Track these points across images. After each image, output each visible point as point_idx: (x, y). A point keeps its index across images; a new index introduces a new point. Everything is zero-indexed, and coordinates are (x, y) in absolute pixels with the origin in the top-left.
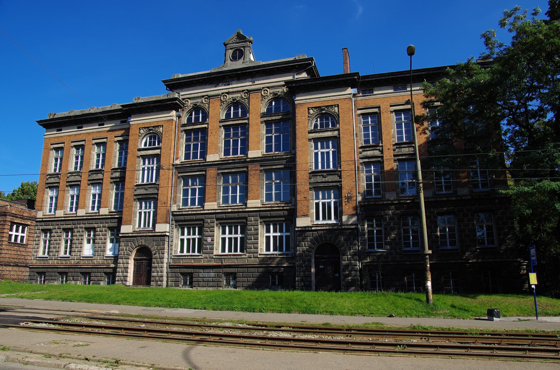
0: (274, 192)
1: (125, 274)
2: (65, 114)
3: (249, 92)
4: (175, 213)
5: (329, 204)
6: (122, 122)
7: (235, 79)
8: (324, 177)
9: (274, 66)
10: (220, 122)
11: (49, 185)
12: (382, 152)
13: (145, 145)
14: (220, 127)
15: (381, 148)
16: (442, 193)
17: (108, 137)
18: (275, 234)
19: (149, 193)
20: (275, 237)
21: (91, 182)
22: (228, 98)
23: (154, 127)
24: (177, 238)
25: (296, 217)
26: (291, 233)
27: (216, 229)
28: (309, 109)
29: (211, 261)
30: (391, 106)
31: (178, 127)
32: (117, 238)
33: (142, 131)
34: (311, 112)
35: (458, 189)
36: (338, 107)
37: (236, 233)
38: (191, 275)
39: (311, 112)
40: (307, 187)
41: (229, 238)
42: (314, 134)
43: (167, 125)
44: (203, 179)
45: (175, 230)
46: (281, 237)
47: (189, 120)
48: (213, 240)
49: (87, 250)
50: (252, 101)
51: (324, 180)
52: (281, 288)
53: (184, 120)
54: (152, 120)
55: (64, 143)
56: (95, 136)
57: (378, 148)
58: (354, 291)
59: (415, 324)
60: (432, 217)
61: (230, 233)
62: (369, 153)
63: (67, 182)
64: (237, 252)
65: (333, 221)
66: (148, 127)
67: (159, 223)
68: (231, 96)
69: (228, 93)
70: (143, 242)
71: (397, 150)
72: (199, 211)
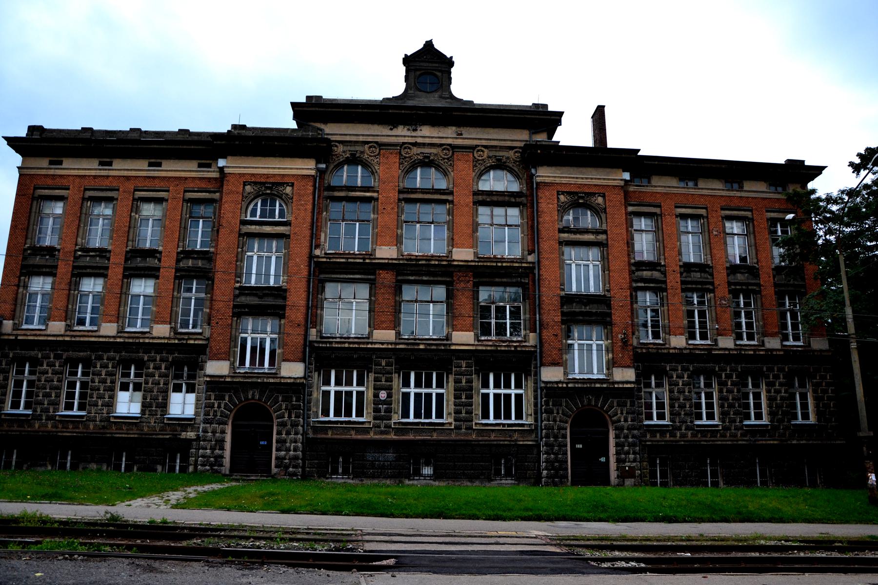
0: (493, 321)
1: (217, 452)
3: (453, 147)
4: (316, 345)
5: (263, 341)
6: (51, 163)
8: (260, 297)
12: (664, 274)
18: (418, 390)
23: (273, 184)
24: (318, 388)
26: (367, 388)
28: (558, 194)
30: (722, 209)
31: (319, 191)
35: (766, 339)
43: (303, 183)
48: (390, 396)
49: (127, 404)
54: (271, 171)
56: (92, 184)
57: (659, 268)
58: (27, 469)
59: (169, 519)
60: (109, 381)
66: (261, 183)
68: (419, 150)
71: (684, 275)
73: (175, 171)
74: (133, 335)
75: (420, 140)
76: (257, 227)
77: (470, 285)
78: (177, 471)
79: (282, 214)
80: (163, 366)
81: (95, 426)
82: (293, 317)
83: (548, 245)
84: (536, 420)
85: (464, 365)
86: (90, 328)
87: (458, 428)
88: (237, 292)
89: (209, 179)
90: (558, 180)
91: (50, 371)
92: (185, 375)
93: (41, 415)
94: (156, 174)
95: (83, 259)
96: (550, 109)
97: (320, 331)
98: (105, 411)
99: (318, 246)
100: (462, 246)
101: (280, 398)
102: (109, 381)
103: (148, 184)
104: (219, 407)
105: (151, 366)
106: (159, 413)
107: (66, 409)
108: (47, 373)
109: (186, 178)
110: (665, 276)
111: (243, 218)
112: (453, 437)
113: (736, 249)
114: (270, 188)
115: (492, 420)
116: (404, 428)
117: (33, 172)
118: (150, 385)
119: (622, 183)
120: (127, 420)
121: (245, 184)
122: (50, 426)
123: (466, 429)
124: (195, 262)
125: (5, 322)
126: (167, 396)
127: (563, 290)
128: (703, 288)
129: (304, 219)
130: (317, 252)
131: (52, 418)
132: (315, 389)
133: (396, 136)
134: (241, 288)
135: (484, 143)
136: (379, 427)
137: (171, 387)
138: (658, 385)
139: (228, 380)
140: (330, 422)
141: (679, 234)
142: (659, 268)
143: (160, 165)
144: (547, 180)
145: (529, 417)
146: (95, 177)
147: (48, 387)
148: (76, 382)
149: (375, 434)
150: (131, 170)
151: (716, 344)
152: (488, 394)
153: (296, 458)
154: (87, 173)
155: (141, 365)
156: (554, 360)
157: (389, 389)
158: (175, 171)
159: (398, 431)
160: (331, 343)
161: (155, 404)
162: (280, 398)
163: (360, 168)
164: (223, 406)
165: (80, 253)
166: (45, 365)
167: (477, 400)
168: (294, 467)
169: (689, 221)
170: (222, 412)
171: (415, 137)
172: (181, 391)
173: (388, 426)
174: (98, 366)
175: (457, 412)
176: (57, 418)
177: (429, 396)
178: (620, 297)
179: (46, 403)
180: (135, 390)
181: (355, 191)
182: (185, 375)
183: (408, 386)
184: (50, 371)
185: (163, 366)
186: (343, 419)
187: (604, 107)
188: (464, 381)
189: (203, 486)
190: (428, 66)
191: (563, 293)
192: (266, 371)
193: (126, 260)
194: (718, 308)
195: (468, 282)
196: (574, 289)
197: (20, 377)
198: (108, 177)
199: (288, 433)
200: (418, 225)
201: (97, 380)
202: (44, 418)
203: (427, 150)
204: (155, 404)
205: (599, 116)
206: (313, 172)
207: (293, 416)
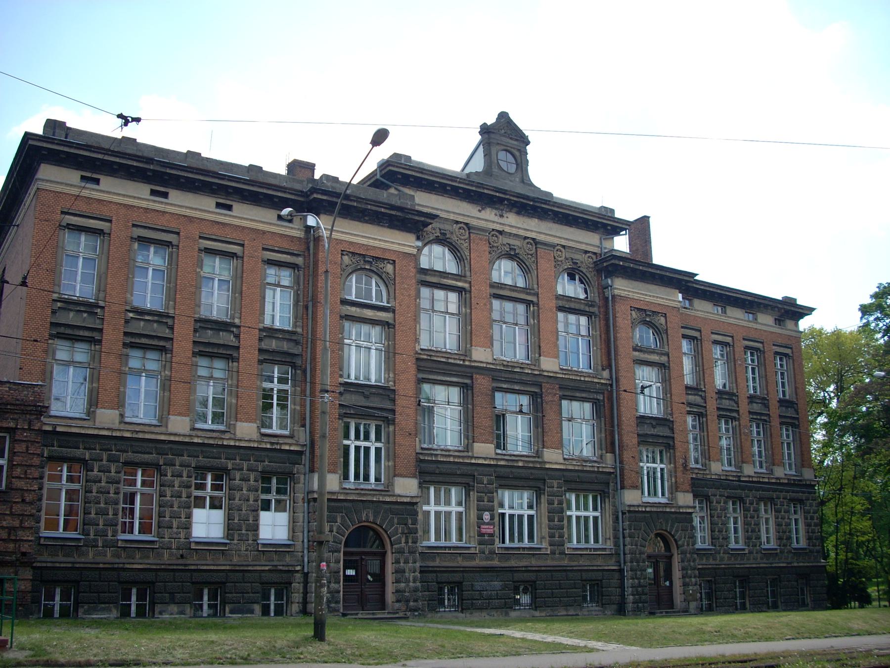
7: (515, 210)
8: (366, 397)
9: (443, 178)
11: (62, 330)
15: (703, 394)
16: (206, 427)
17: (246, 242)
18: (579, 513)
19: (371, 405)
22: (500, 241)
29: (492, 559)
30: (744, 339)
36: (665, 317)
37: (448, 503)
38: (459, 584)
40: (635, 441)
46: (596, 519)
49: (207, 524)
52: (535, 605)
55: (110, 221)
56: (143, 220)
57: (700, 393)
60: (184, 495)
65: (660, 499)
69: (501, 232)
70: (368, 516)
72: (459, 457)
73: (251, 220)
75: (507, 229)
76: (358, 310)
80: (252, 478)
81: (171, 555)
83: (326, 317)
84: (616, 544)
85: (556, 486)
87: (553, 553)
89: (292, 238)
90: (631, 295)
91: (104, 479)
93: (96, 541)
94: (227, 220)
95: (134, 323)
96: (617, 215)
97: (122, 416)
98: (182, 535)
101: (396, 520)
102: (184, 495)
103: (82, 207)
105: (238, 477)
106: (251, 538)
108: (100, 481)
109: (264, 232)
112: (549, 562)
113: (719, 378)
116: (508, 554)
117: (59, 188)
118: (237, 501)
122: (109, 555)
123: (560, 554)
128: (229, 354)
129: (408, 307)
131: (114, 544)
133: (486, 220)
135: (563, 242)
138: (795, 512)
141: (264, 286)
142: (700, 393)
143: (165, 195)
144: (623, 294)
145: (608, 541)
147: (102, 501)
148: (205, 498)
149: (481, 560)
150: (196, 209)
151: (772, 474)
153: (416, 590)
154: (136, 203)
155: (220, 474)
158: (251, 220)
160: (436, 455)
161: (241, 526)
162: (396, 520)
164: (335, 529)
165: (131, 315)
166: (96, 470)
168: (416, 601)
169: (217, 260)
170: (334, 537)
171: (503, 224)
173: (492, 552)
174: (169, 474)
175: (552, 536)
178: (405, 387)
179: (101, 523)
180: (213, 507)
181: (447, 278)
184: (104, 479)
185: (252, 478)
187: (649, 217)
188: (556, 502)
190: (503, 137)
192: (373, 487)
194: (743, 436)
195: (555, 394)
196: (353, 376)
198: (164, 213)
199: (406, 562)
201: (169, 493)
202: (100, 544)
203: (512, 241)
204: (241, 526)
207: (410, 541)
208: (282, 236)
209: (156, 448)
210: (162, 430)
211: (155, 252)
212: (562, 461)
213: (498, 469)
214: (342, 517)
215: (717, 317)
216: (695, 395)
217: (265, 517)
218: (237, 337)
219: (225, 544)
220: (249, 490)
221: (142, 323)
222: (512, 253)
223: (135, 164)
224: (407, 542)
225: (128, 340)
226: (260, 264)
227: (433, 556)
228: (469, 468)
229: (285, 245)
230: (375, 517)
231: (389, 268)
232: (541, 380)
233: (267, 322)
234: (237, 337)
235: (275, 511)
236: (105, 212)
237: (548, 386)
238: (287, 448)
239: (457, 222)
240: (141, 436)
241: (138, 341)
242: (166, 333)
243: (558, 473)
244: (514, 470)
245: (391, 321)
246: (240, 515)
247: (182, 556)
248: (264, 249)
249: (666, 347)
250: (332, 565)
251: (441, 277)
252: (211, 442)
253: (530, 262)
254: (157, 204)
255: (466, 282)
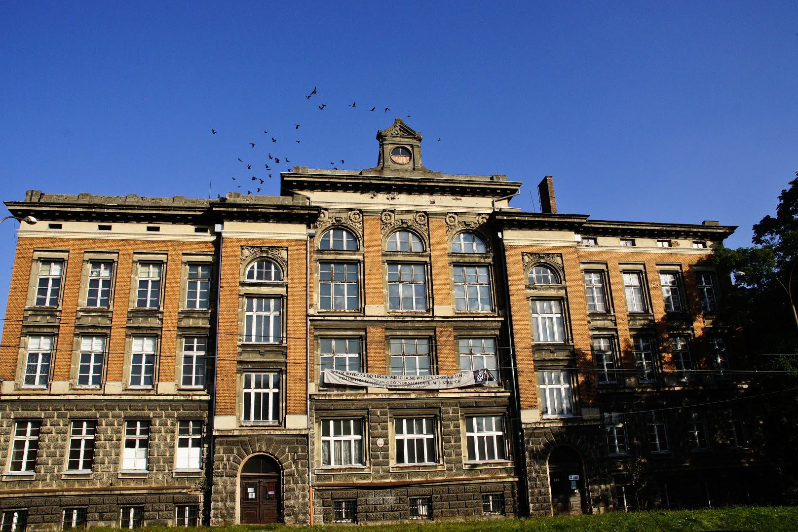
2: (70, 195)
4: (316, 398)
8: (262, 354)
10: (383, 255)
11: (31, 330)
13: (251, 275)
14: (384, 262)
15: (613, 318)
18: (411, 437)
20: (410, 442)
21: (134, 331)
23: (269, 248)
24: (319, 438)
25: (520, 408)
27: (390, 424)
29: (386, 477)
32: (208, 440)
33: (246, 252)
34: (526, 258)
36: (561, 257)
39: (526, 258)
40: (531, 366)
41: (479, 437)
42: (532, 291)
44: (432, 340)
45: (316, 425)
46: (431, 442)
47: (325, 242)
48: (386, 443)
49: (133, 460)
50: (434, 230)
51: (552, 356)
53: (317, 242)
56: (140, 249)
60: (115, 439)
61: (410, 431)
62: (600, 323)
63: (76, 327)
64: (403, 462)
67: (293, 414)
69: (393, 211)
70: (261, 448)
74: (137, 393)
75: (398, 208)
77: (451, 338)
78: (131, 527)
79: (278, 276)
82: (294, 372)
86: (93, 387)
87: (450, 469)
88: (240, 350)
90: (522, 243)
92: (191, 430)
99: (311, 305)
100: (442, 303)
102: (115, 439)
103: (49, 245)
104: (228, 460)
107: (71, 467)
108: (51, 433)
109: (184, 242)
110: (616, 325)
111: (242, 280)
114: (266, 252)
115: (406, 463)
119: (575, 244)
120: (133, 476)
121: (242, 248)
124: (196, 321)
125: (5, 383)
126: (173, 451)
127: (533, 340)
130: (311, 311)
132: (316, 440)
134: (243, 346)
135: (455, 210)
136: (378, 472)
137: (177, 442)
139: (236, 433)
140: (332, 470)
146: (95, 240)
149: (375, 478)
152: (473, 438)
156: (530, 403)
157: (386, 436)
159: (395, 475)
163: (345, 233)
165: (81, 314)
167: (464, 443)
170: (231, 465)
172: (187, 446)
174: (104, 424)
176: (63, 477)
177: (420, 441)
179: (50, 462)
180: (140, 446)
181: (343, 254)
182: (191, 430)
183: (401, 432)
186: (416, 464)
189: (490, 522)
191: (533, 343)
192: (271, 424)
193: (129, 319)
195: (449, 335)
197: (22, 438)
200: (401, 285)
202: (48, 478)
203: (404, 217)
205: (544, 188)
206: (305, 237)
208: (198, 243)
209: (389, 404)
210: (102, 392)
211: (105, 269)
212: (177, 392)
213: (391, 402)
214: (238, 449)
215: (623, 250)
216: (604, 320)
217: (180, 452)
218: (162, 320)
219: (146, 474)
220: (166, 432)
221: (90, 319)
222: (405, 226)
223: (82, 210)
224: (297, 467)
225: (78, 331)
226: (580, 274)
227: (328, 477)
228: (363, 403)
229: (201, 249)
230: (268, 447)
231: (284, 254)
232: (434, 324)
233: (630, 310)
234: (162, 320)
235: (193, 446)
236: (65, 246)
237: (441, 329)
238: (197, 398)
239: (351, 210)
240: (82, 397)
241: (86, 331)
242: (108, 323)
243: (455, 401)
244: (407, 402)
245: (285, 294)
246: (158, 452)
247: (111, 484)
248: (184, 254)
249: (563, 282)
250: (228, 487)
251: (337, 254)
252: (136, 398)
253: (423, 230)
254: (104, 235)
255: (360, 254)
